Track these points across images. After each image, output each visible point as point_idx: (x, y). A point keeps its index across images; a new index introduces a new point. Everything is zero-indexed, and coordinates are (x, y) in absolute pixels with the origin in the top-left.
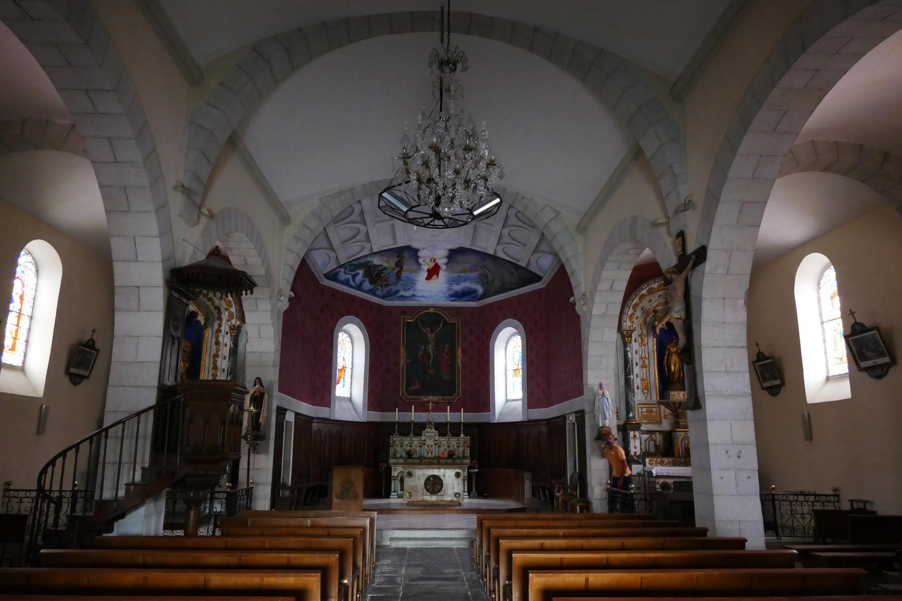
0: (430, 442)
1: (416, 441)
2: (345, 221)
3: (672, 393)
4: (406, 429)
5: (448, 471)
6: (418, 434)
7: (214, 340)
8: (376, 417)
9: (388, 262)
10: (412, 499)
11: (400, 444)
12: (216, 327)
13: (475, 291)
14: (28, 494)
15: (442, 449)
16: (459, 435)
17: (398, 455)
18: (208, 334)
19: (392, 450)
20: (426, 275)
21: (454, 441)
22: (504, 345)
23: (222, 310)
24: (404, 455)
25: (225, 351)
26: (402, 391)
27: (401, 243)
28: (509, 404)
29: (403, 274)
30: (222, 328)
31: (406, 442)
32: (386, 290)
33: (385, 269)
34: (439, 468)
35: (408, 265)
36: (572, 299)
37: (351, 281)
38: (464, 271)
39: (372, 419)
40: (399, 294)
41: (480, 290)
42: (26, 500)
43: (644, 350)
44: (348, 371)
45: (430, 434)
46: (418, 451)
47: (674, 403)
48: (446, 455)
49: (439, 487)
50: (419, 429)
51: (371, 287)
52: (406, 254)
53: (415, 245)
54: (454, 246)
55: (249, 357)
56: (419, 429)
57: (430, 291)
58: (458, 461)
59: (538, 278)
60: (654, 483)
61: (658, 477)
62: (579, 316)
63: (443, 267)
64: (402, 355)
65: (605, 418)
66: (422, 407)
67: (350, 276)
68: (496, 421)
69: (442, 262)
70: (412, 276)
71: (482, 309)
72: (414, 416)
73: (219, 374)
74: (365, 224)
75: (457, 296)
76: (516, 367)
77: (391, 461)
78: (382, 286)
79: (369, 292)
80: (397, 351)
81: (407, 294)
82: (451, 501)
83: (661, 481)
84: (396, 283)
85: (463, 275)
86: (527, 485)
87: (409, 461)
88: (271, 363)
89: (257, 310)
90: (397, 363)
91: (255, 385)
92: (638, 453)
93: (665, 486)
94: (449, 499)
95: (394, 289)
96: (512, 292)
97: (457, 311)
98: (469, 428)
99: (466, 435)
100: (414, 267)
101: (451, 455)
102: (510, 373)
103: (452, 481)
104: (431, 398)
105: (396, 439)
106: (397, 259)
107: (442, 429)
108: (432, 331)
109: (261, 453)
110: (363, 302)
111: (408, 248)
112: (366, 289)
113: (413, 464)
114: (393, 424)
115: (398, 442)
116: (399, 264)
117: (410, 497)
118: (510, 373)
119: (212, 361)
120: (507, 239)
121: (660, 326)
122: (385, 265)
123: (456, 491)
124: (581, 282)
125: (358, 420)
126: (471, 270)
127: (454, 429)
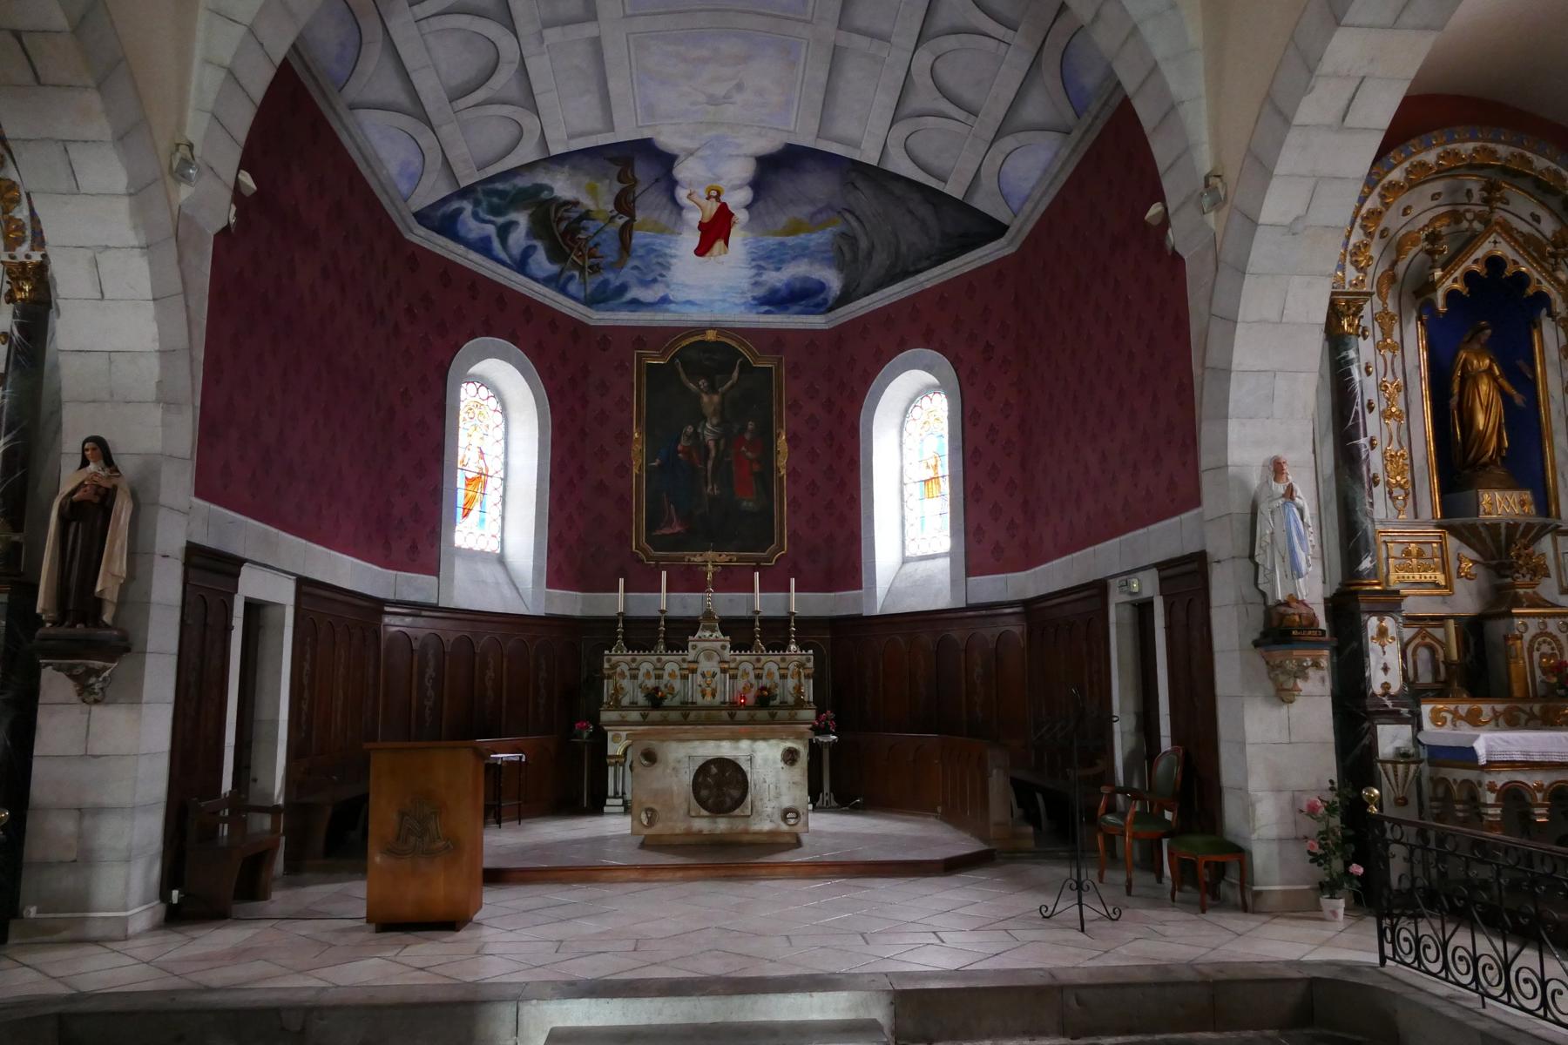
0: (707, 666)
2: (480, 95)
3: (1486, 497)
4: (643, 634)
5: (761, 745)
8: (570, 603)
9: (593, 192)
10: (658, 829)
11: (631, 675)
13: (822, 287)
15: (740, 683)
16: (784, 647)
17: (625, 701)
19: (608, 687)
20: (692, 239)
21: (771, 663)
22: (897, 421)
26: (638, 539)
27: (625, 132)
28: (909, 567)
29: (639, 238)
31: (645, 667)
32: (593, 281)
33: (587, 215)
34: (735, 738)
35: (648, 209)
36: (1155, 209)
37: (496, 244)
38: (793, 229)
39: (558, 610)
40: (629, 296)
41: (833, 281)
43: (1391, 366)
44: (494, 484)
45: (709, 646)
46: (692, 690)
47: (1493, 528)
48: (751, 698)
49: (736, 793)
50: (679, 632)
51: (554, 268)
53: (667, 139)
54: (768, 144)
57: (708, 287)
58: (782, 714)
59: (996, 229)
60: (1472, 789)
61: (1491, 765)
62: (1177, 260)
63: (741, 216)
64: (637, 447)
65: (1295, 571)
66: (689, 580)
67: (491, 230)
68: (878, 610)
69: (737, 199)
71: (839, 335)
72: (664, 602)
74: (510, 24)
75: (776, 300)
76: (930, 473)
77: (606, 716)
78: (582, 270)
79: (548, 281)
80: (624, 438)
82: (771, 833)
83: (1501, 779)
84: (617, 266)
85: (790, 240)
86: (997, 782)
87: (655, 715)
88: (150, 391)
89: (77, 191)
90: (624, 470)
91: (85, 463)
92: (1394, 690)
93: (1513, 796)
94: (767, 826)
95: (615, 280)
96: (921, 277)
97: (776, 340)
98: (809, 630)
99: (803, 646)
100: (665, 217)
101: (764, 699)
102: (914, 490)
103: (770, 765)
104: (710, 554)
105: (618, 658)
106: (617, 187)
107: (740, 632)
108: (712, 389)
109: (114, 702)
110: (531, 308)
111: (645, 148)
112: (541, 275)
113: (664, 722)
114: (608, 623)
115: (624, 667)
116: (625, 204)
117: (651, 822)
118: (914, 490)
120: (925, 96)
121: (1449, 282)
122: (587, 202)
123: (786, 802)
124: (1192, 136)
125: (523, 611)
126: (812, 225)
127: (775, 633)
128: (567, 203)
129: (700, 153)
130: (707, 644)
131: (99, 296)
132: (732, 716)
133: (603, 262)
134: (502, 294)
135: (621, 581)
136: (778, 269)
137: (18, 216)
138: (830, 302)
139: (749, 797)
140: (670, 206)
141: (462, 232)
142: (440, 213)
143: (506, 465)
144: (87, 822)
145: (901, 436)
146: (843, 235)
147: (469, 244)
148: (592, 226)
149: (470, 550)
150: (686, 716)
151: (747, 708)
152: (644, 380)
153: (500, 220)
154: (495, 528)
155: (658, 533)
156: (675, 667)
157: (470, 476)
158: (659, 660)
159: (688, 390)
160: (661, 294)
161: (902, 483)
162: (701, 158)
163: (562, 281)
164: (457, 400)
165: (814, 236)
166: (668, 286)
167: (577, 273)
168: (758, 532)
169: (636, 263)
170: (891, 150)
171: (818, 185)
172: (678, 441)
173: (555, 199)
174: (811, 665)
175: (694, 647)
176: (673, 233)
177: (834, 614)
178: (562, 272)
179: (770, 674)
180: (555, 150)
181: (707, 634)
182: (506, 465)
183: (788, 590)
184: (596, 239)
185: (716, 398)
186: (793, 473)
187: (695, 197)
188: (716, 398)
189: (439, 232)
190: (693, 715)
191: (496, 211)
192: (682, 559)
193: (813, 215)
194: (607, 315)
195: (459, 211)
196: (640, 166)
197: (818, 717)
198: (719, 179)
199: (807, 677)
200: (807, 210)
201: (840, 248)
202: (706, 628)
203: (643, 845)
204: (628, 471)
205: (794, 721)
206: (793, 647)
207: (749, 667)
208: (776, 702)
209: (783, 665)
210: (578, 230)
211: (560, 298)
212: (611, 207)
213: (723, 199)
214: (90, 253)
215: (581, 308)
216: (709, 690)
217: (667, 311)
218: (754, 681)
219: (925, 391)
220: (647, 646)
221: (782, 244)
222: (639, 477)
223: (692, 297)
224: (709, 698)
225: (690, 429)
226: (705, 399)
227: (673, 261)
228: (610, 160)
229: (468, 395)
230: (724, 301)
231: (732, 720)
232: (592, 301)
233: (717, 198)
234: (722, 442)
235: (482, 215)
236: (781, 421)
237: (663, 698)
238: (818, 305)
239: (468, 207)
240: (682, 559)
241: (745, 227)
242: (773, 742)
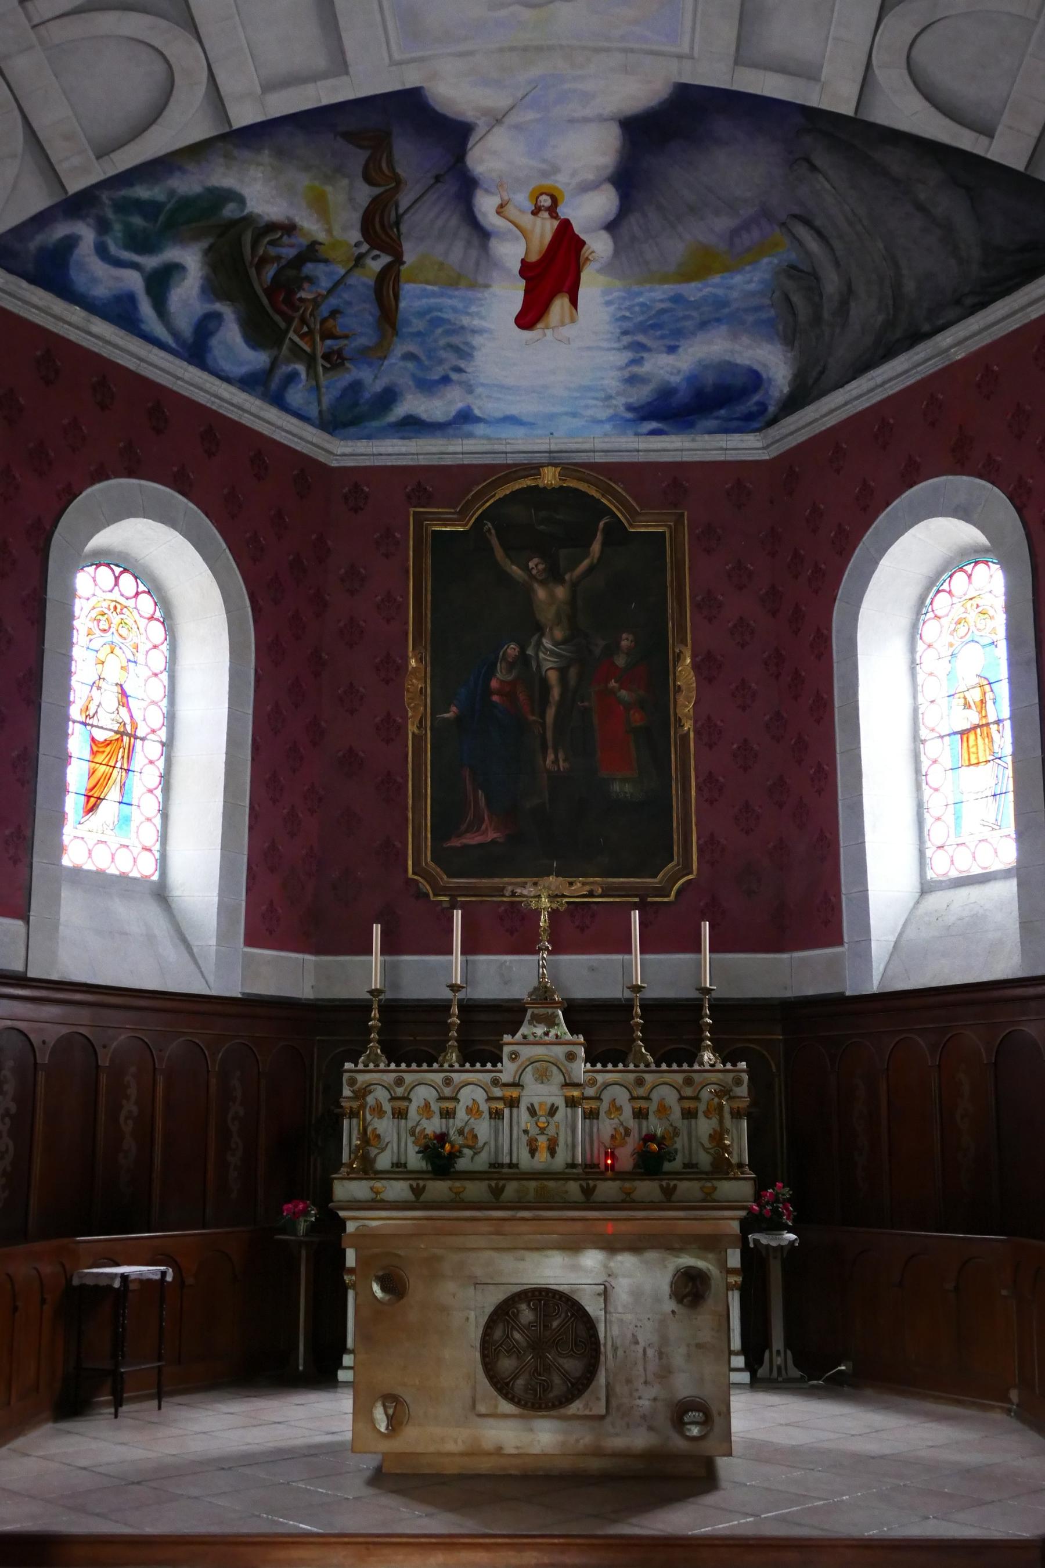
0: (541, 1093)
1: (473, 1087)
4: (413, 1032)
6: (481, 1052)
8: (291, 975)
9: (319, 205)
11: (395, 1106)
13: (755, 380)
15: (606, 1127)
16: (692, 1057)
17: (384, 1161)
19: (350, 1134)
20: (510, 295)
21: (665, 1086)
22: (904, 620)
24: (414, 1160)
26: (417, 853)
27: (370, 77)
28: (936, 901)
29: (413, 297)
31: (422, 1094)
32: (334, 385)
33: (312, 252)
34: (573, 1246)
35: (427, 239)
37: (146, 308)
38: (698, 267)
39: (267, 987)
40: (400, 411)
41: (775, 364)
44: (148, 751)
45: (543, 1063)
46: (489, 1139)
48: (626, 1158)
49: (573, 1366)
50: (482, 1030)
51: (258, 359)
52: (410, 158)
53: (454, 92)
54: (639, 90)
56: (482, 1030)
57: (543, 385)
58: (686, 1188)
63: (599, 246)
64: (414, 683)
66: (505, 930)
67: (134, 281)
68: (875, 985)
69: (590, 210)
70: (449, 302)
71: (788, 468)
72: (450, 972)
75: (668, 410)
76: (973, 717)
77: (345, 1189)
78: (310, 361)
79: (249, 383)
80: (392, 669)
81: (433, 408)
84: (375, 354)
85: (693, 290)
87: (438, 1188)
90: (391, 728)
95: (373, 381)
96: (945, 339)
97: (673, 482)
98: (738, 1022)
99: (729, 1056)
100: (457, 253)
101: (652, 1160)
105: (371, 1078)
106: (365, 194)
107: (603, 1028)
108: (554, 575)
110: (215, 430)
111: (410, 109)
113: (457, 1203)
115: (381, 1095)
116: (381, 228)
117: (395, 1423)
122: (311, 226)
125: (197, 987)
127: (670, 1028)
128: (272, 227)
129: (513, 119)
130: (539, 1051)
132: (588, 1192)
133: (350, 346)
134: (158, 404)
135: (377, 929)
136: (672, 349)
138: (772, 409)
139: (601, 1378)
140: (464, 232)
141: (79, 280)
142: (33, 245)
143: (171, 719)
145: (913, 650)
146: (792, 270)
147: (91, 306)
148: (323, 275)
149: (100, 874)
150: (497, 1192)
151: (620, 1176)
153: (151, 262)
154: (150, 835)
155: (456, 843)
156: (480, 1095)
157: (101, 736)
158: (448, 1082)
159: (504, 578)
160: (460, 405)
161: (917, 741)
162: (518, 127)
163: (274, 386)
164: (70, 594)
165: (738, 279)
166: (470, 389)
167: (301, 368)
168: (637, 839)
169: (412, 347)
170: (880, 74)
171: (739, 170)
172: (491, 672)
173: (248, 220)
174: (743, 1090)
175: (514, 1056)
176: (473, 286)
177: (788, 994)
178: (274, 364)
179: (663, 1110)
180: (243, 115)
181: (540, 1030)
182: (171, 719)
183: (697, 949)
184: (333, 301)
185: (561, 592)
186: (707, 728)
187: (511, 211)
188: (561, 592)
189: (33, 280)
190: (511, 1189)
191: (141, 243)
192: (500, 891)
193: (735, 233)
194: (362, 446)
195: (70, 243)
196: (402, 145)
197: (758, 1198)
198: (556, 170)
199: (736, 1115)
200: (723, 223)
201: (787, 299)
202: (537, 1019)
203: (382, 1478)
204: (401, 729)
205: (709, 1202)
206: (707, 1056)
207: (622, 1096)
208: (677, 1165)
209: (688, 1092)
210: (302, 280)
211: (272, 413)
212: (355, 236)
213: (564, 212)
215: (311, 433)
216: (542, 1141)
217: (470, 435)
218: (631, 1123)
219: (964, 558)
220: (427, 1056)
221: (677, 299)
222: (418, 739)
223: (514, 410)
224: (543, 1156)
225: (512, 649)
226: (541, 593)
227: (477, 340)
228: (350, 137)
229: (91, 590)
230: (574, 415)
231: (589, 1201)
232: (335, 422)
233: (553, 211)
234: (573, 672)
235: (113, 249)
236: (681, 627)
237: (454, 1156)
238: (749, 417)
239: (86, 233)
240: (500, 891)
241: (608, 269)
242: (651, 1255)
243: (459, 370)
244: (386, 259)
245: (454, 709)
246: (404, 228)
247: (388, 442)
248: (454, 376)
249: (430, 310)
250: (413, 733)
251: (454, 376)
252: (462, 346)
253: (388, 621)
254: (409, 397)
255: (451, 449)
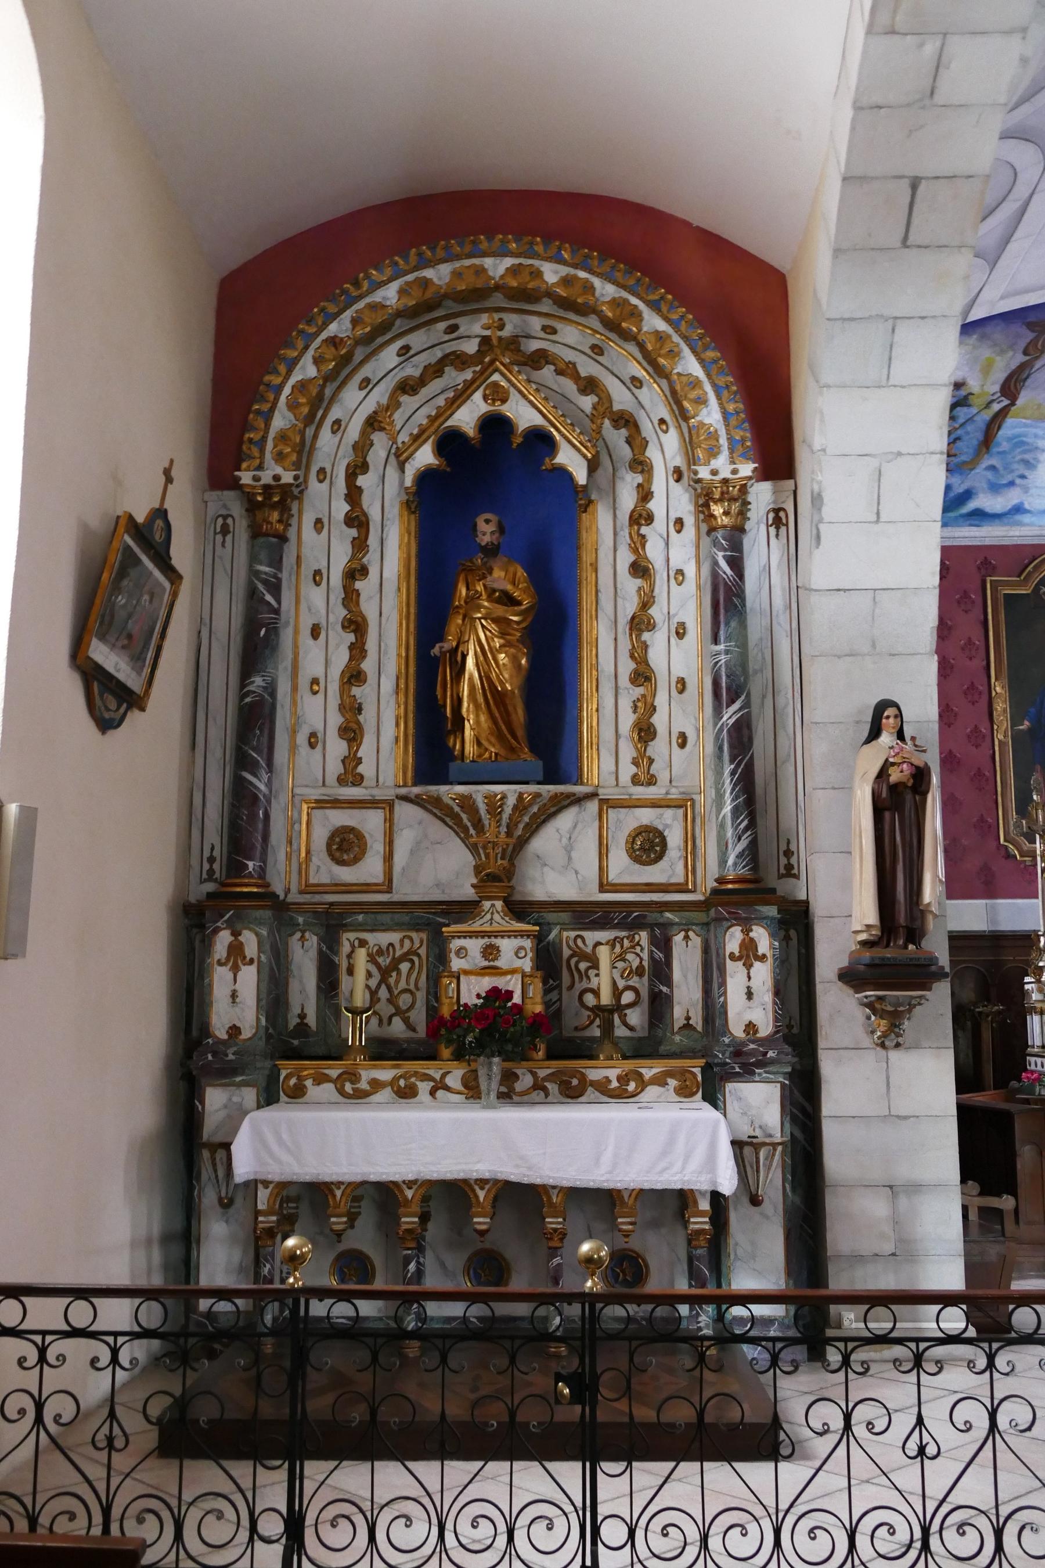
7: (626, 558)
12: (627, 500)
14: (81, 1314)
18: (604, 530)
23: (647, 429)
25: (684, 602)
29: (1010, 427)
30: (657, 505)
40: (972, 505)
42: (77, 1349)
55: (823, 617)
73: (661, 700)
89: (885, 384)
91: (875, 733)
109: (917, 1046)
119: (625, 645)
131: (874, 518)
137: (707, 421)
144: (903, 1201)
152: (1002, 617)
160: (1015, 501)
169: (993, 461)
212: (997, 388)
214: (874, 463)
217: (1020, 524)
243: (1023, 477)
244: (1006, 402)
245: (1027, 723)
246: (1027, 384)
247: (963, 529)
248: (1018, 481)
249: (1019, 436)
250: (1000, 741)
251: (1018, 481)
252: (1032, 461)
253: (971, 659)
254: (981, 495)
255: (1011, 533)
